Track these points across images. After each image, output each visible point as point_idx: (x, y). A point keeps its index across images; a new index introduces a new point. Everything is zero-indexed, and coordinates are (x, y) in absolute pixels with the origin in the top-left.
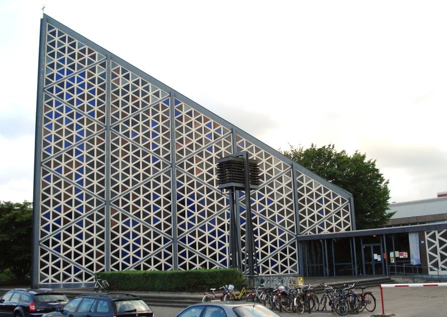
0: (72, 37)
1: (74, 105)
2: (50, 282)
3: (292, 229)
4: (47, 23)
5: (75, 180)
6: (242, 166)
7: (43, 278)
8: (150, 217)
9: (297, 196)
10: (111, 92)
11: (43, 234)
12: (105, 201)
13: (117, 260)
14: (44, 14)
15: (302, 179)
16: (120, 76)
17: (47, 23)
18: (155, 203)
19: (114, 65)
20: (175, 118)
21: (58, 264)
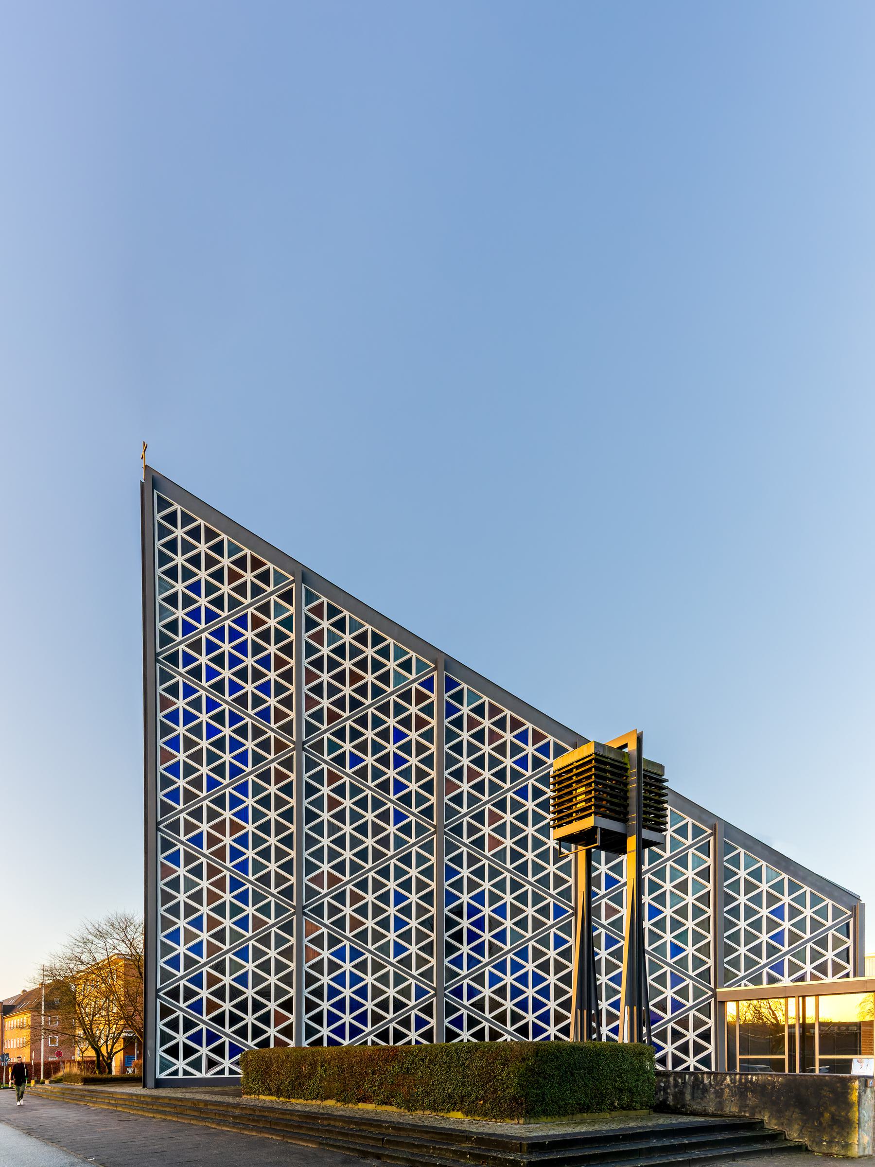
0: (215, 527)
1: (462, 1000)
2: (181, 1075)
3: (428, 974)
4: (155, 487)
5: (231, 862)
6: (622, 802)
7: (165, 1065)
8: (231, 846)
9: (721, 900)
10: (305, 662)
11: (166, 976)
12: (305, 914)
13: (320, 1031)
14: (147, 468)
15: (735, 861)
16: (325, 624)
17: (155, 487)
18: (354, 855)
19: (310, 597)
20: (446, 721)
21: (197, 1038)
